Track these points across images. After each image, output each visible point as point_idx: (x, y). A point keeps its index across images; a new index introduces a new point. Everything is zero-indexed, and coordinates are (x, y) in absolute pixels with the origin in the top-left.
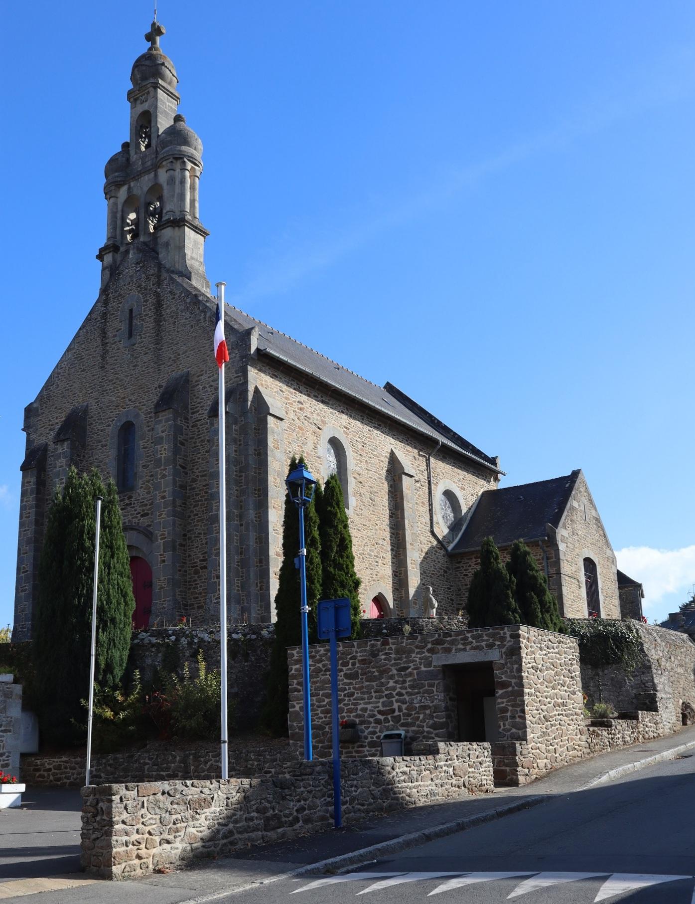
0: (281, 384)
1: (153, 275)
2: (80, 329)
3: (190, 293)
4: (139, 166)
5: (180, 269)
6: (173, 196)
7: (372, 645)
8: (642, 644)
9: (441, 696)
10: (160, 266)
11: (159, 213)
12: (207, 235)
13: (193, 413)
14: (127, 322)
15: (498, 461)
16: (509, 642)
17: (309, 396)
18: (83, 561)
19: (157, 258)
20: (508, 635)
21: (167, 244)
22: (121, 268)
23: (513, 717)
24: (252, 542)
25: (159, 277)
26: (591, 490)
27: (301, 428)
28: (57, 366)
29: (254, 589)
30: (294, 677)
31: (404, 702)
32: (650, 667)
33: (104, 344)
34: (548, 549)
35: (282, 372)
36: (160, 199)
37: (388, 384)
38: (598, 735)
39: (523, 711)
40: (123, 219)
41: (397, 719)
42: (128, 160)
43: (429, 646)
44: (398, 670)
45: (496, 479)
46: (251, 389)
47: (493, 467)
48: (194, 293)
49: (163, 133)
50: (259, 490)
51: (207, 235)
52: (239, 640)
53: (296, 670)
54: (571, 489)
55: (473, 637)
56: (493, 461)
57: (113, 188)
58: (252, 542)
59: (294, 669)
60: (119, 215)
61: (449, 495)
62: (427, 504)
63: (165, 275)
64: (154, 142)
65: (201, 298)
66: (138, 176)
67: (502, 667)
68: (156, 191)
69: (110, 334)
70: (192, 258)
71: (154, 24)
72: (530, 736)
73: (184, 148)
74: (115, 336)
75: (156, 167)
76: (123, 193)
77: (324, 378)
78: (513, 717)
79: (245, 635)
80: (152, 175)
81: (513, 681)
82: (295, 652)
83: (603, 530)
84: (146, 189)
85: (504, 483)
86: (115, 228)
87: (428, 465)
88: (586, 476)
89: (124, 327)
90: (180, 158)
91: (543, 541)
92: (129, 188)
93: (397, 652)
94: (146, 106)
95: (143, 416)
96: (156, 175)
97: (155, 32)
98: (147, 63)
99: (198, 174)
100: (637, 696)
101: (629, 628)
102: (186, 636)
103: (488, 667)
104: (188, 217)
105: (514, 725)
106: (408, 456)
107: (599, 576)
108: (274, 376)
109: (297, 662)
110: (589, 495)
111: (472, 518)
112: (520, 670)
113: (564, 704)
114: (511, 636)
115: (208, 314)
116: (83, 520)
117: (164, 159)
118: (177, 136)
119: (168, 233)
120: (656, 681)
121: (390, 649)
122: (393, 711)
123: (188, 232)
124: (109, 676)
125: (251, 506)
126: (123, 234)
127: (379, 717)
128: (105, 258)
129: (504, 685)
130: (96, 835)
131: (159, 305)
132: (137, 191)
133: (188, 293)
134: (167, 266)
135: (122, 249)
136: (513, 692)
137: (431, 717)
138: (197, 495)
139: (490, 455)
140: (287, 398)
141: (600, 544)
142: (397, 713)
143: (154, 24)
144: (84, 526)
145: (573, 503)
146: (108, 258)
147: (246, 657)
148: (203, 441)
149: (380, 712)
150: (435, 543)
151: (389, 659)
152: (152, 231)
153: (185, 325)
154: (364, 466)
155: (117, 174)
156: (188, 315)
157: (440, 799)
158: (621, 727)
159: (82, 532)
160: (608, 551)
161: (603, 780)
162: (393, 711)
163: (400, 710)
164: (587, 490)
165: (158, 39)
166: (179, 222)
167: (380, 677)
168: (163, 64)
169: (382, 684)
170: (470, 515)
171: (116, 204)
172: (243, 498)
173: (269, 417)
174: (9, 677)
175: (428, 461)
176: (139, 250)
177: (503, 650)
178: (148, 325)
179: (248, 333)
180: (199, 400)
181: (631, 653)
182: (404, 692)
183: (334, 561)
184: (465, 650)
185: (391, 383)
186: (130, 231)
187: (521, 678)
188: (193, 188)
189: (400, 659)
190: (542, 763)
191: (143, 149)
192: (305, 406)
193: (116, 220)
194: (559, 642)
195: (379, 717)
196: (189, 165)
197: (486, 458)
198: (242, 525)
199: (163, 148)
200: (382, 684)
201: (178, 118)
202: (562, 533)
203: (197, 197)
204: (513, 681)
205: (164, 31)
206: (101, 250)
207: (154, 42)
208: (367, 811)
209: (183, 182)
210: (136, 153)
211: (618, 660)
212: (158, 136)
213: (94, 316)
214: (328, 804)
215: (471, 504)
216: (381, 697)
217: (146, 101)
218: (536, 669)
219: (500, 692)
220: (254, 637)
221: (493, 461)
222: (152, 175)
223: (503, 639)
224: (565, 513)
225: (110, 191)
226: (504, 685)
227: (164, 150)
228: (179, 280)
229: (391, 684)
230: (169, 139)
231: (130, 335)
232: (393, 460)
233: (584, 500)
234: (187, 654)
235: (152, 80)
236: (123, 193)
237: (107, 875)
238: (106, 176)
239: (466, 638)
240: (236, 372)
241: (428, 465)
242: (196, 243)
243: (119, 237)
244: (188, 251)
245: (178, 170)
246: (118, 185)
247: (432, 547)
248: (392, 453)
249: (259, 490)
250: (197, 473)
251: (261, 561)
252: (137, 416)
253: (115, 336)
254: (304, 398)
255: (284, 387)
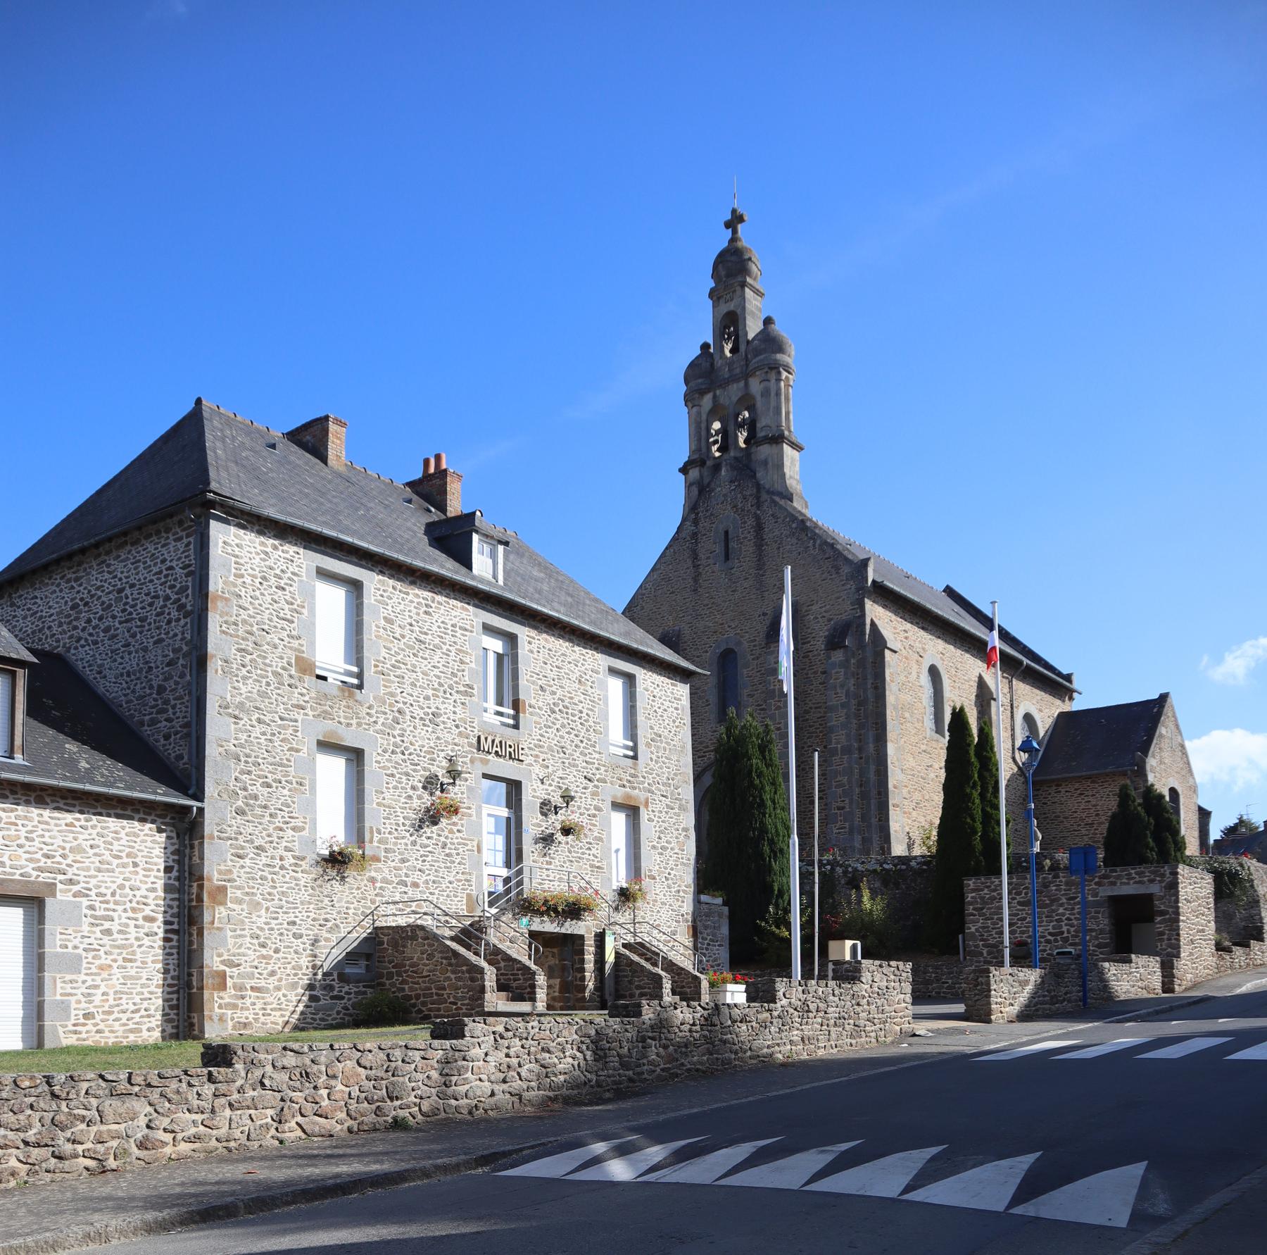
0: (890, 614)
1: (751, 495)
2: (667, 548)
3: (796, 518)
4: (725, 373)
5: (780, 489)
6: (769, 409)
7: (1044, 878)
8: (1252, 880)
9: (1106, 921)
10: (758, 487)
11: (752, 425)
12: (802, 449)
13: (803, 644)
14: (723, 544)
15: (1074, 678)
16: (1168, 878)
17: (912, 623)
18: (754, 798)
19: (754, 476)
20: (1168, 872)
21: (765, 463)
22: (713, 485)
23: (1169, 939)
24: (872, 776)
25: (758, 498)
26: (1178, 715)
27: (906, 658)
28: (641, 586)
29: (874, 821)
30: (971, 903)
31: (1072, 926)
32: (1258, 902)
33: (696, 567)
34: (1137, 779)
35: (892, 601)
36: (751, 408)
37: (948, 587)
38: (1223, 959)
39: (1178, 935)
40: (708, 428)
41: (1066, 940)
42: (712, 365)
43: (1097, 880)
44: (1068, 899)
45: (1071, 698)
46: (868, 622)
47: (1068, 684)
48: (800, 518)
49: (754, 339)
50: (876, 724)
51: (802, 449)
52: (891, 870)
53: (972, 898)
54: (1159, 714)
55: (1136, 873)
56: (1068, 678)
57: (697, 396)
58: (872, 776)
59: (969, 897)
60: (703, 426)
61: (1028, 718)
62: (1009, 728)
63: (764, 496)
64: (743, 347)
65: (808, 524)
66: (725, 384)
67: (1161, 898)
68: (747, 401)
69: (701, 555)
70: (791, 477)
71: (734, 211)
72: (1182, 955)
73: (779, 356)
74: (708, 558)
75: (746, 376)
76: (707, 401)
77: (929, 606)
78: (1169, 939)
79: (895, 865)
80: (742, 384)
81: (1171, 910)
82: (971, 882)
83: (1187, 757)
84: (735, 399)
85: (1079, 704)
86: (699, 440)
87: (1011, 688)
88: (1174, 700)
89: (719, 549)
90: (775, 368)
91: (1133, 771)
92: (715, 397)
93: (1067, 884)
94: (731, 306)
95: (746, 645)
96: (747, 385)
97: (735, 220)
98: (733, 258)
99: (791, 383)
100: (1245, 928)
101: (1241, 865)
102: (841, 866)
103: (1149, 898)
104: (786, 433)
105: (1170, 946)
106: (995, 679)
107: (1182, 807)
108: (885, 607)
109: (973, 891)
110: (1176, 720)
111: (1049, 741)
112: (1177, 901)
113: (1203, 931)
114: (1171, 873)
115: (818, 542)
116: (750, 759)
117: (758, 369)
118: (770, 342)
119: (764, 451)
120: (1263, 915)
121: (1061, 881)
122: (1062, 933)
123: (787, 449)
124: (780, 901)
125: (871, 740)
126: (709, 450)
127: (1049, 937)
128: (691, 471)
129: (1163, 913)
130: (977, 997)
131: (759, 528)
132: (723, 400)
133: (794, 518)
134: (767, 487)
135: (709, 463)
136: (1170, 920)
137: (1097, 938)
138: (810, 726)
139: (1065, 672)
140: (895, 628)
141: (1183, 773)
142: (1065, 935)
143: (734, 211)
144: (752, 765)
145: (1162, 730)
146: (694, 473)
147: (897, 885)
148: (815, 673)
149: (1050, 934)
150: (1016, 769)
151: (1060, 890)
152: (743, 445)
153: (790, 552)
154: (957, 692)
155: (700, 381)
156: (794, 541)
157: (1132, 996)
158: (1238, 951)
159: (750, 772)
160: (1191, 779)
161: (1243, 990)
162: (1062, 933)
163: (1069, 932)
164: (1174, 716)
165: (739, 226)
166: (778, 439)
167: (1051, 904)
168: (750, 259)
169: (1053, 911)
170: (1047, 738)
171: (699, 413)
172: (862, 732)
173: (886, 651)
174: (719, 901)
175: (1011, 682)
176: (733, 468)
177: (1163, 885)
178: (748, 548)
179: (865, 563)
180: (809, 631)
181: (1243, 889)
182: (1072, 917)
183: (990, 801)
184: (1128, 884)
185: (951, 585)
186: (716, 442)
187: (1178, 908)
188: (787, 399)
189: (1070, 890)
190: (1189, 976)
191: (728, 354)
192: (909, 634)
193: (699, 433)
194: (1202, 878)
195: (1049, 937)
196: (784, 374)
197: (1059, 674)
198: (861, 758)
199: (756, 356)
200: (1053, 911)
201: (768, 321)
202: (1151, 762)
203: (791, 409)
204: (1171, 910)
205: (746, 218)
206: (686, 464)
207: (735, 232)
208: (1096, 999)
209: (778, 394)
210: (721, 358)
211: (1231, 894)
212: (748, 342)
213: (683, 535)
214: (1079, 991)
215: (1047, 726)
216: (1052, 921)
217: (732, 300)
218: (1188, 901)
219: (1159, 919)
220: (904, 867)
221: (1068, 678)
222: (742, 384)
223: (1163, 875)
224: (1155, 741)
225: (691, 399)
226: (1163, 913)
227: (757, 359)
228: (782, 502)
229: (1061, 910)
230: (763, 346)
231: (727, 557)
232: (981, 684)
233: (1171, 725)
234: (843, 882)
235: (740, 279)
236: (707, 401)
237: (989, 1021)
238: (687, 381)
239: (1130, 874)
240: (852, 604)
241: (1011, 688)
242: (793, 460)
243: (704, 450)
244: (786, 470)
245: (773, 381)
246: (702, 393)
247: (1013, 775)
248: (980, 677)
249: (876, 724)
250: (811, 705)
251: (879, 793)
252: (739, 643)
253: (708, 558)
254: (908, 626)
255: (893, 617)
